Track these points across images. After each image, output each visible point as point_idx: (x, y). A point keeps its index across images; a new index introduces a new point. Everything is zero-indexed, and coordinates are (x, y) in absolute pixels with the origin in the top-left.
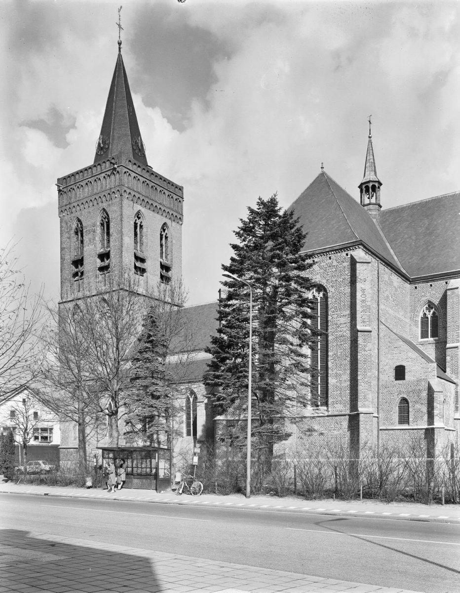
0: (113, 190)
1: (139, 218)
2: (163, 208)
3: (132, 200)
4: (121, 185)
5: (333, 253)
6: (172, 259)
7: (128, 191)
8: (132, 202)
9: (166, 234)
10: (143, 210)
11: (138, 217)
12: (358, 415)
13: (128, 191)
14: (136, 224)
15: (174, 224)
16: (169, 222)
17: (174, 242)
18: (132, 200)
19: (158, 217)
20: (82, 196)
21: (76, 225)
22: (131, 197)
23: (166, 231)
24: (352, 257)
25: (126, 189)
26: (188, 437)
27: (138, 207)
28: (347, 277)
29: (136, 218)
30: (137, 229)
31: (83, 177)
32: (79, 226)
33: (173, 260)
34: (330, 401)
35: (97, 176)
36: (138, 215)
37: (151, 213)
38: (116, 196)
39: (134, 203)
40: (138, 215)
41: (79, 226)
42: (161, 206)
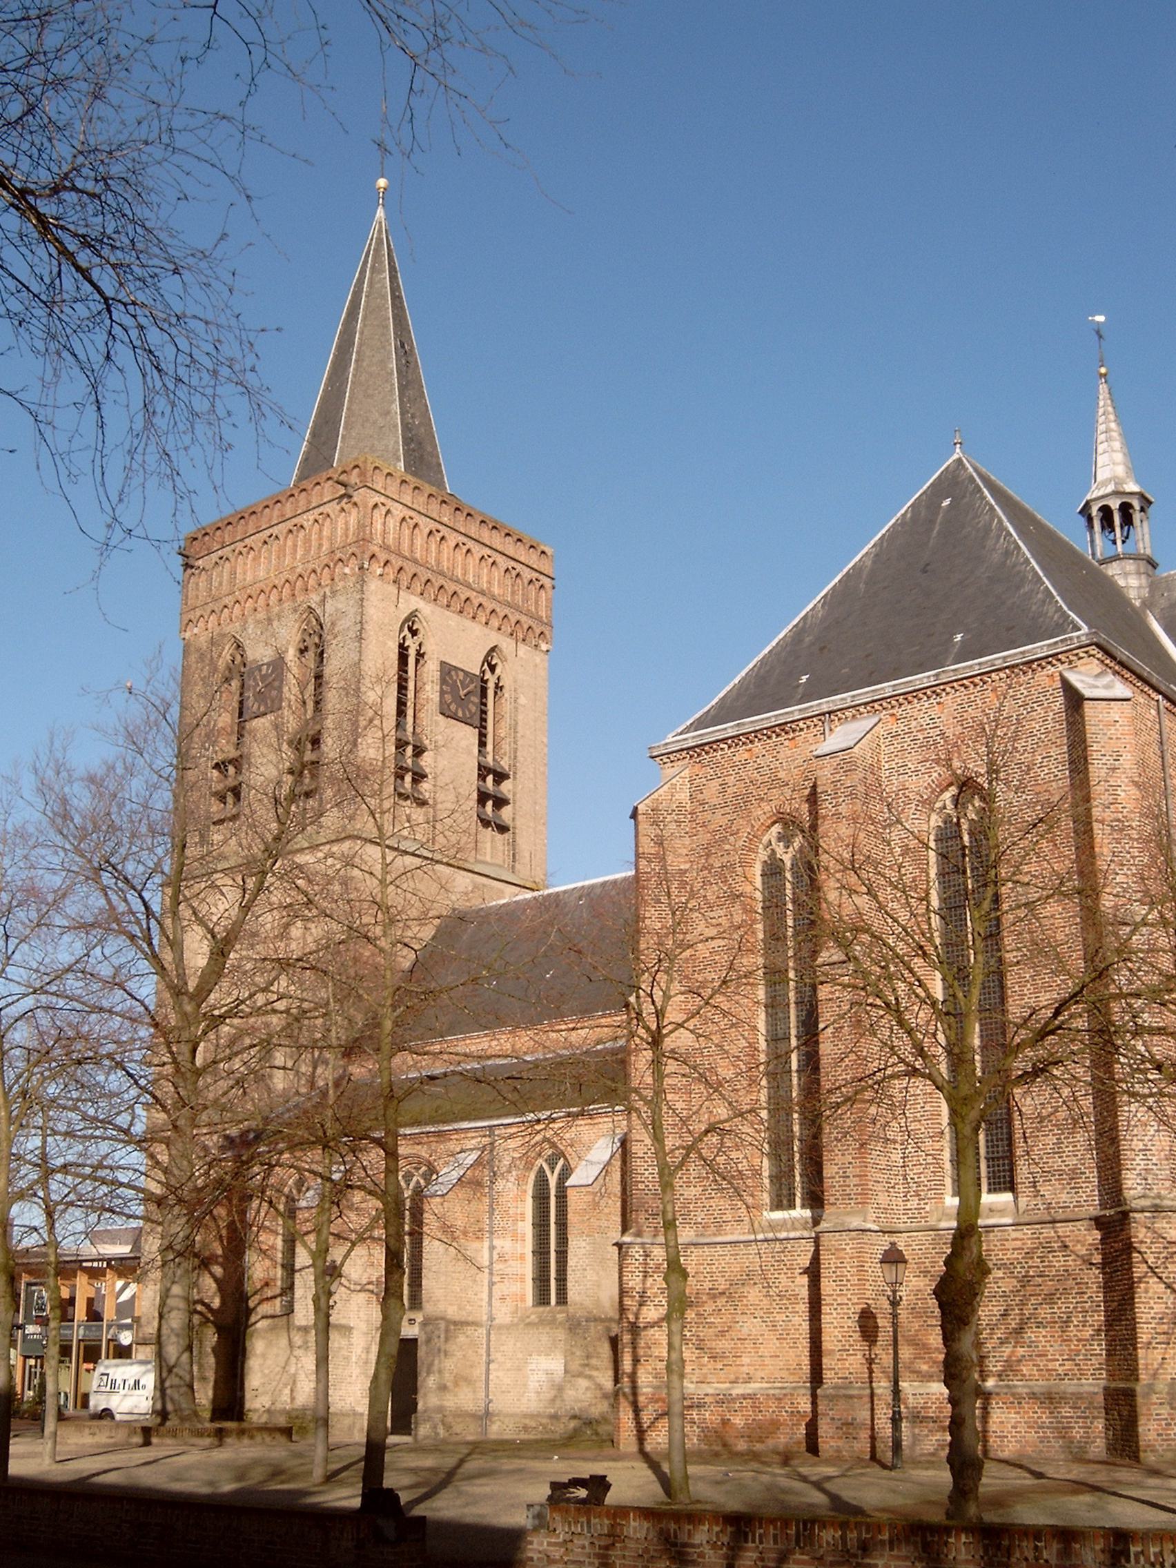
0: (339, 555)
1: (414, 633)
2: (490, 606)
3: (394, 582)
4: (363, 539)
5: (1002, 675)
6: (516, 751)
7: (383, 556)
8: (392, 589)
9: (498, 679)
10: (426, 609)
11: (410, 629)
12: (1125, 1215)
13: (383, 556)
14: (403, 650)
15: (523, 649)
16: (507, 645)
17: (522, 700)
18: (394, 582)
19: (476, 629)
20: (249, 578)
21: (229, 657)
22: (391, 572)
23: (498, 671)
24: (1068, 688)
25: (376, 549)
26: (541, 1309)
27: (411, 602)
28: (1054, 752)
29: (406, 631)
30: (406, 665)
31: (309, 502)
32: (238, 658)
33: (519, 754)
34: (1023, 1171)
35: (295, 521)
36: (411, 626)
37: (453, 619)
38: (347, 570)
39: (399, 588)
40: (411, 626)
41: (238, 658)
42: (481, 599)
